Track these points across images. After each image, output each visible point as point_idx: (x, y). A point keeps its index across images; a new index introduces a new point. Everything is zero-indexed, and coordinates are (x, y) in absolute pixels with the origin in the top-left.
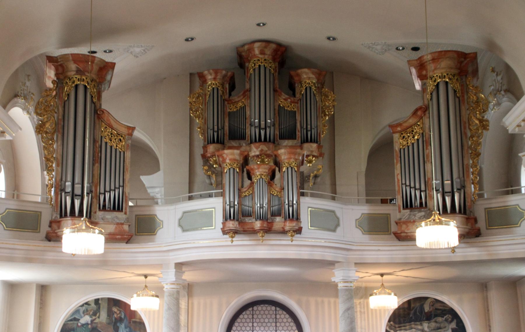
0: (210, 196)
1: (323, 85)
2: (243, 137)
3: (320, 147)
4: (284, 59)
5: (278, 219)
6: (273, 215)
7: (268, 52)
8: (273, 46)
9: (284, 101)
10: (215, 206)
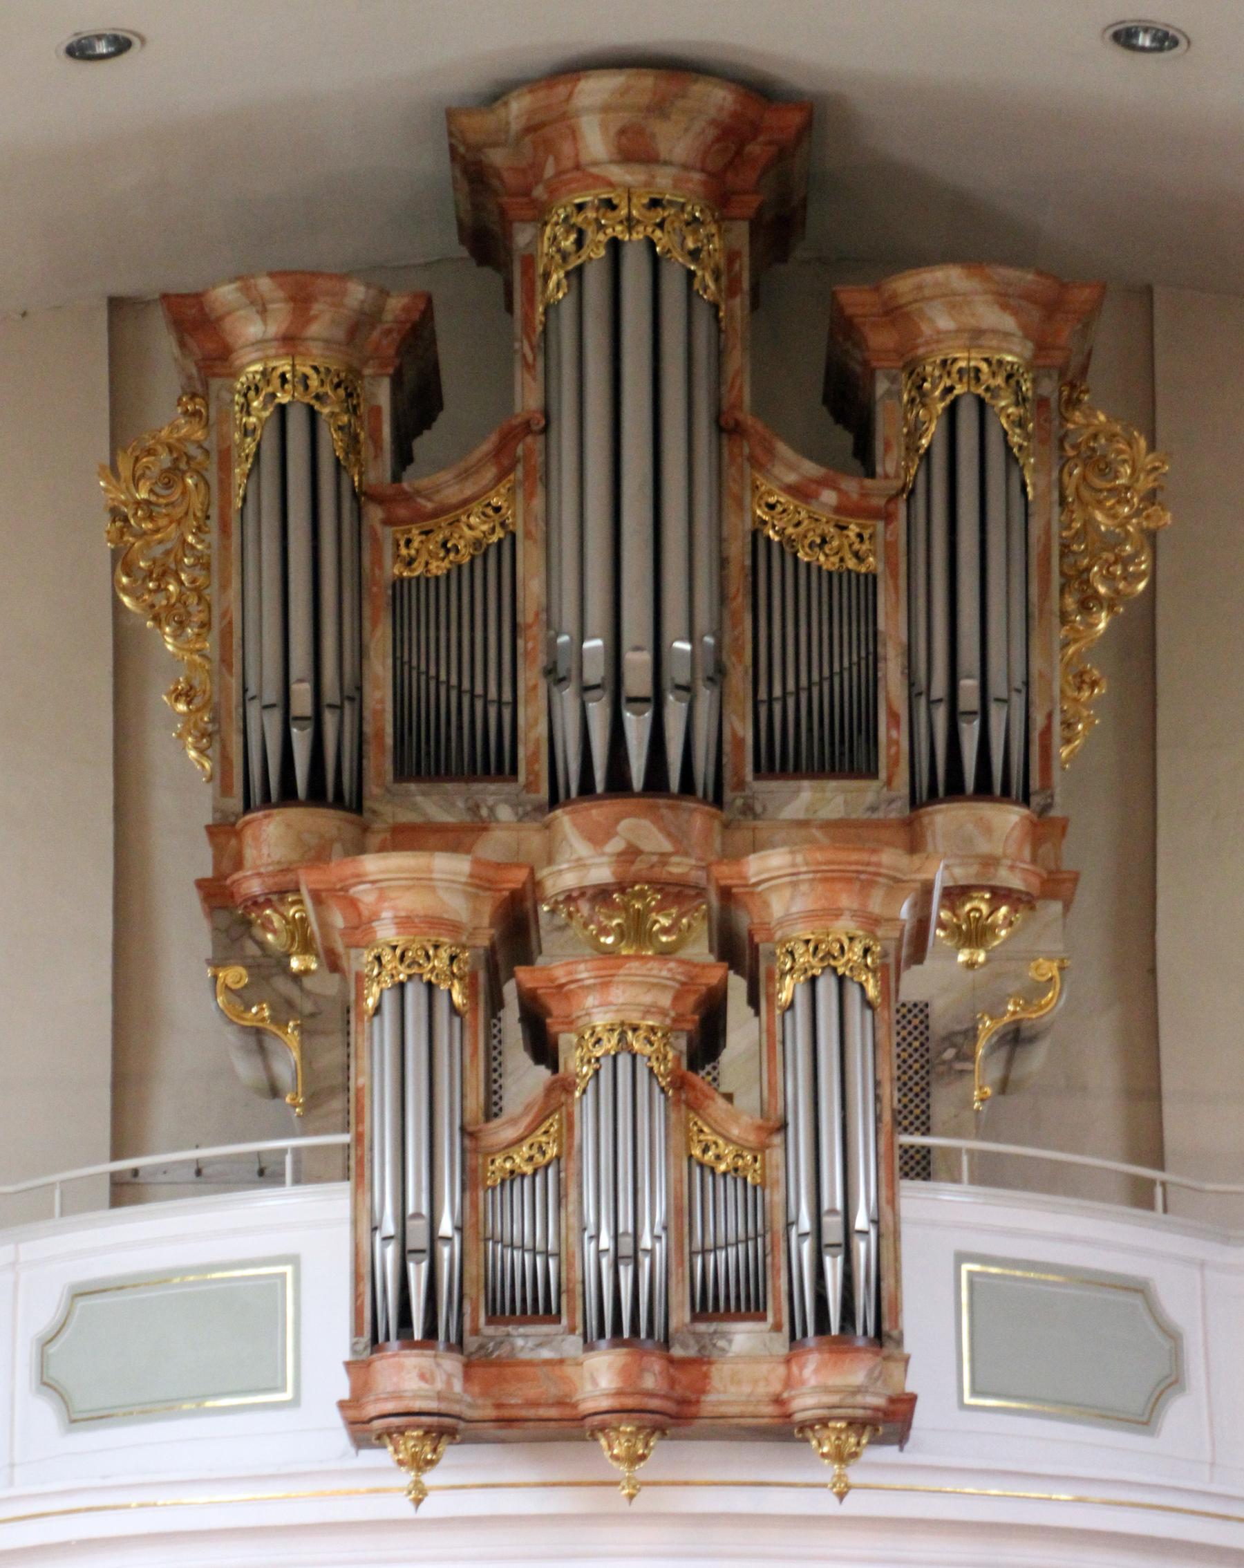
0: (265, 1173)
1: (1073, 384)
2: (496, 763)
3: (1045, 829)
4: (785, 183)
5: (743, 1338)
6: (710, 1307)
7: (679, 141)
8: (717, 99)
9: (793, 497)
10: (301, 1244)
